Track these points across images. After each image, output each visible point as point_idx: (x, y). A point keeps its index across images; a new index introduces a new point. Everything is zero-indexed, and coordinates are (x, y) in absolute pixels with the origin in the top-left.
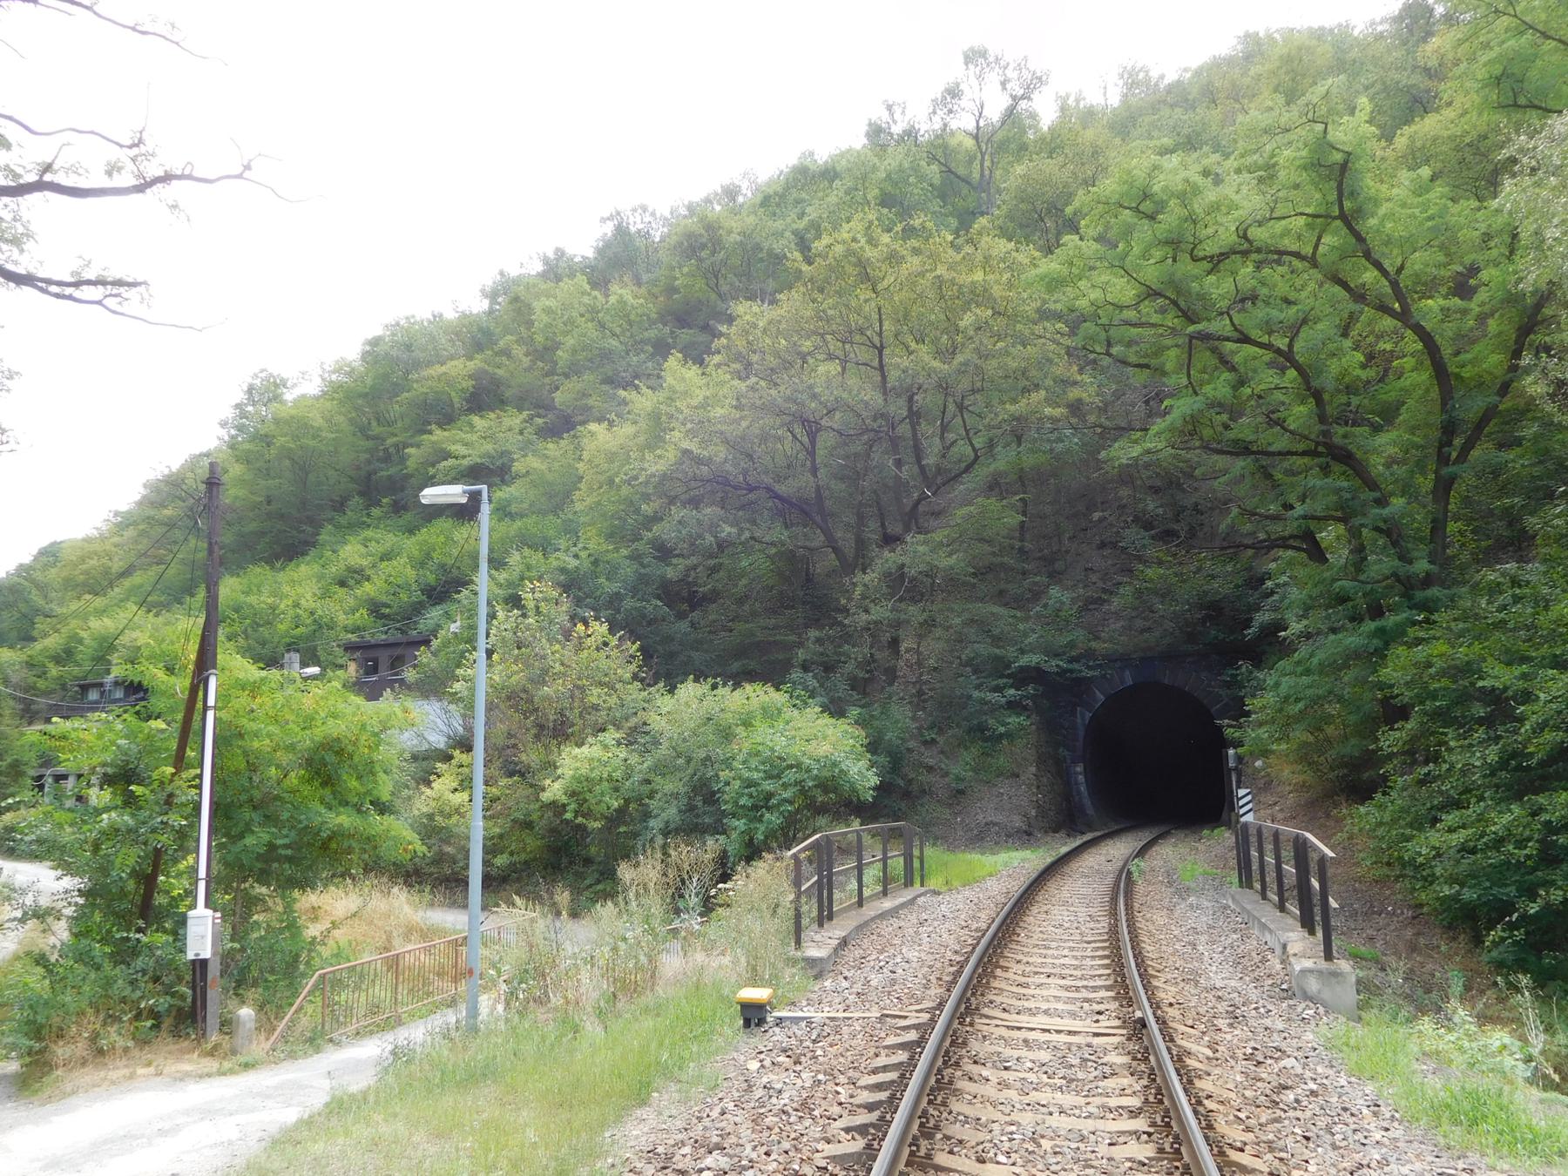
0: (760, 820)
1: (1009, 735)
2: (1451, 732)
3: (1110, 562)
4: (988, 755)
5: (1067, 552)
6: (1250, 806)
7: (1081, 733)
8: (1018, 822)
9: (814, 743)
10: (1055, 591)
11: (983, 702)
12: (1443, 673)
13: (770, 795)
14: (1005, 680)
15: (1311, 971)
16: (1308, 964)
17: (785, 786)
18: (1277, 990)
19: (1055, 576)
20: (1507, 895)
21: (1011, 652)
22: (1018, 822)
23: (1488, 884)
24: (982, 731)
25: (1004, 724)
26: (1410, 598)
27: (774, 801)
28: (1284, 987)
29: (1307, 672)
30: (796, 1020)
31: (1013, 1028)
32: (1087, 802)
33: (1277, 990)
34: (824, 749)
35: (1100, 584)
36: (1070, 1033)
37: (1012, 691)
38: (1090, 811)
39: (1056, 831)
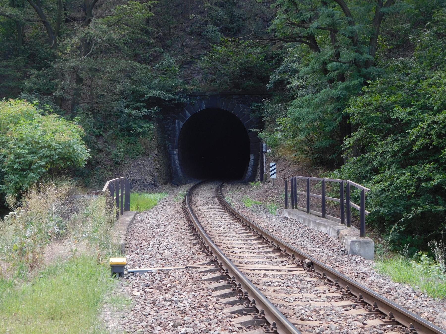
0: (26, 176)
1: (143, 133)
2: (378, 137)
3: (195, 42)
4: (131, 144)
5: (172, 35)
6: (275, 171)
7: (178, 133)
8: (149, 179)
9: (57, 134)
10: (166, 56)
11: (130, 115)
12: (377, 109)
13: (31, 163)
14: (141, 104)
15: (356, 242)
16: (354, 239)
17: (41, 158)
18: (340, 251)
19: (167, 48)
20: (399, 210)
21: (144, 88)
22: (149, 179)
23: (392, 206)
24: (129, 131)
25: (142, 127)
26: (359, 72)
27: (34, 166)
28: (343, 249)
29: (309, 106)
30: (142, 272)
31: (251, 270)
32: (179, 169)
33: (340, 251)
34: (64, 138)
35: (190, 54)
36: (277, 270)
37: (146, 110)
38: (180, 174)
39: (166, 184)
